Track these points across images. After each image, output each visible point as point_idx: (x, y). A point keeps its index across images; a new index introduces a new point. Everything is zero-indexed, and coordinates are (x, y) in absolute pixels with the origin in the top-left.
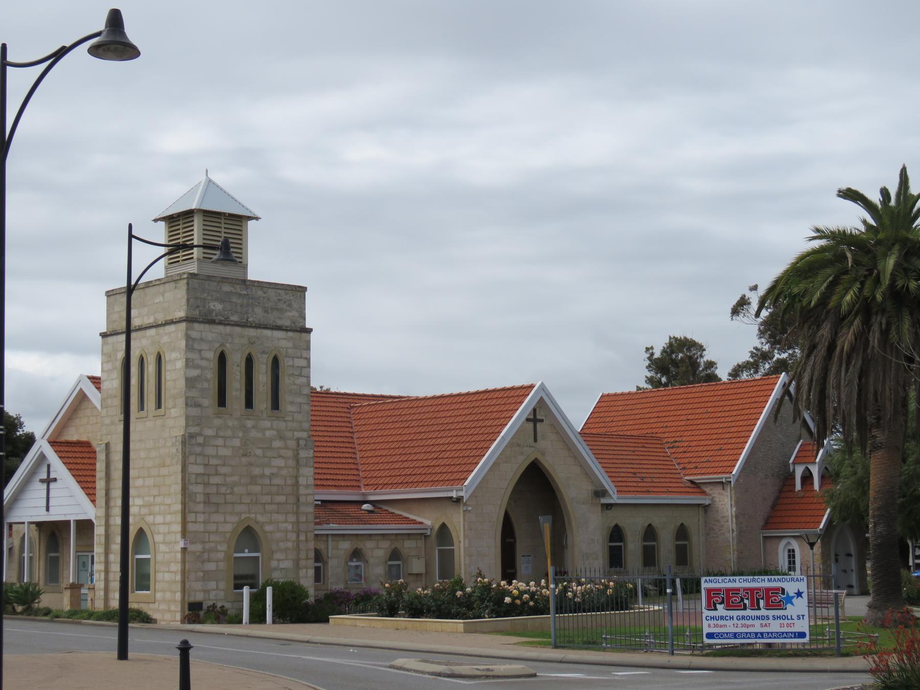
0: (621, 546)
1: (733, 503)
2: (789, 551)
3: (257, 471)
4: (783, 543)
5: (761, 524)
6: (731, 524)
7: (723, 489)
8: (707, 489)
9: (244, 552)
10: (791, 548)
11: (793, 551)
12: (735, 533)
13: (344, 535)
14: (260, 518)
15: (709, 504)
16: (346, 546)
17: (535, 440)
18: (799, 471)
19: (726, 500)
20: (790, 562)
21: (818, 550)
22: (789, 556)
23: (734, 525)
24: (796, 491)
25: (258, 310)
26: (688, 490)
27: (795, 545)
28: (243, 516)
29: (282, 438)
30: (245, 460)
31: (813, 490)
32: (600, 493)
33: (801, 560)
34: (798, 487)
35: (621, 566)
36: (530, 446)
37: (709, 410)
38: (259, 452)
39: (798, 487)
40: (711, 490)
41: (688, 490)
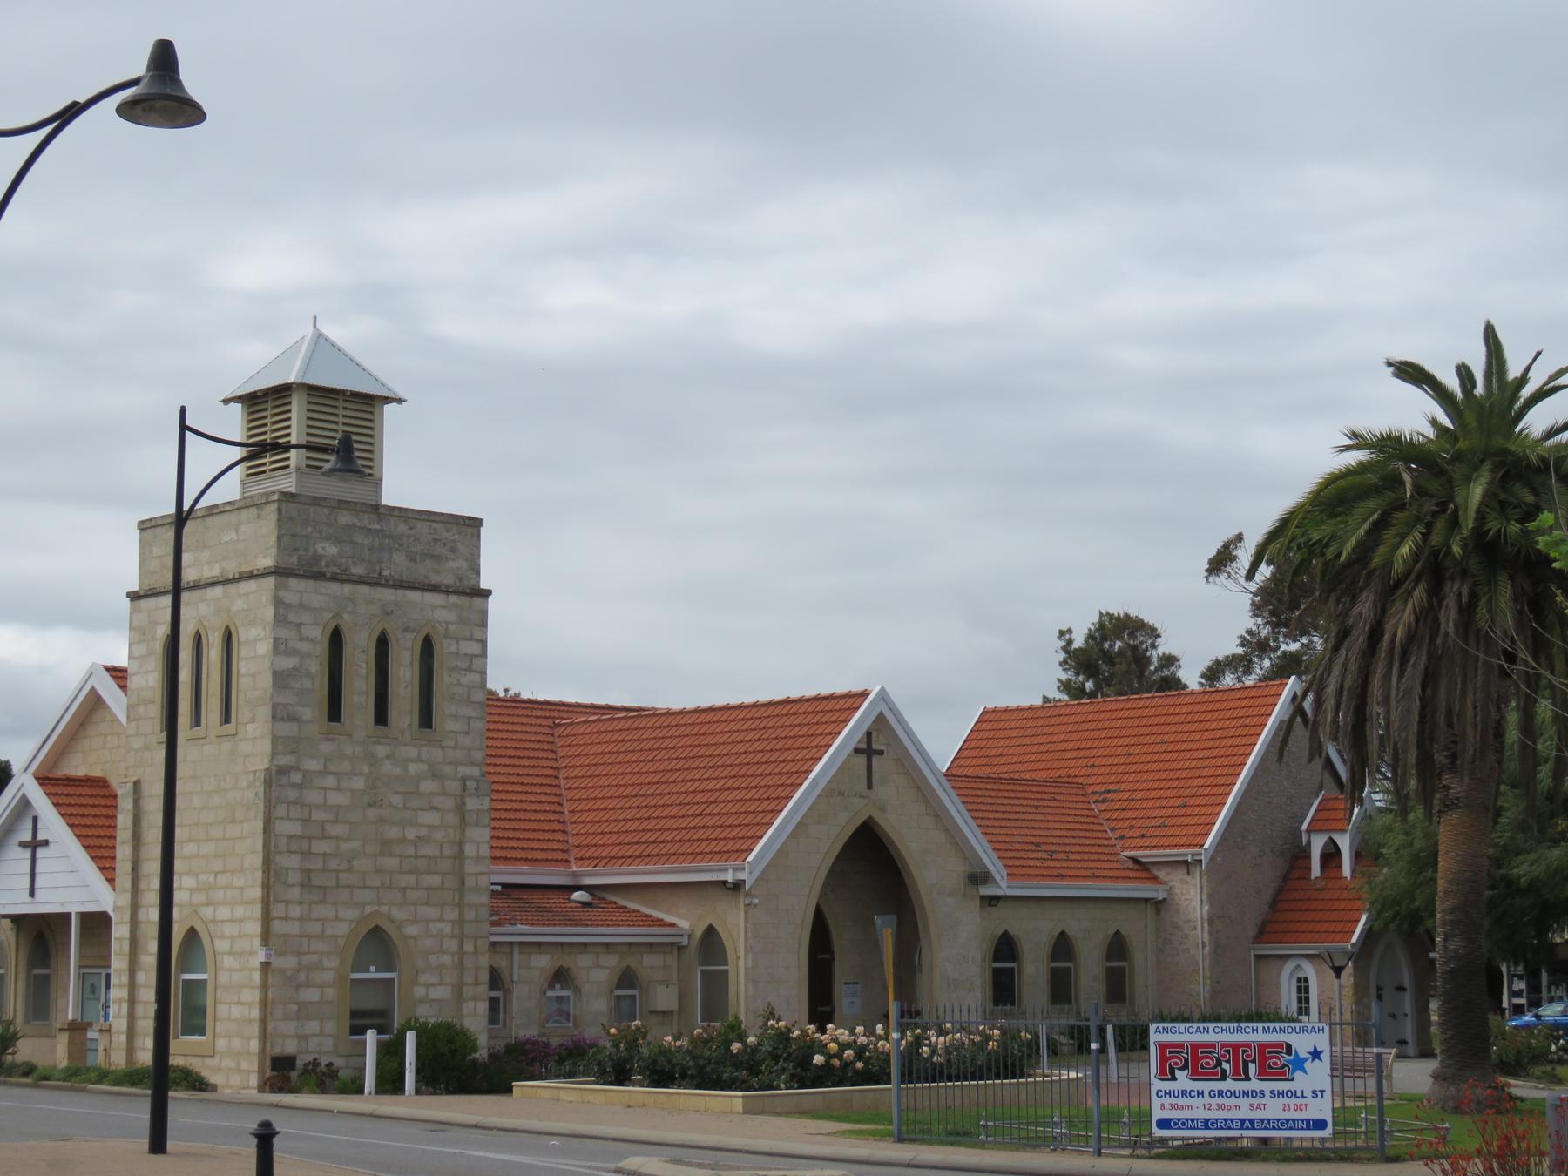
0: (1013, 969)
1: (1205, 897)
2: (1299, 980)
3: (393, 832)
4: (1290, 966)
5: (1252, 932)
6: (1201, 934)
7: (1189, 873)
8: (1161, 874)
9: (368, 971)
10: (1301, 975)
11: (1306, 980)
12: (1207, 948)
13: (539, 944)
14: (397, 914)
15: (1164, 899)
16: (543, 963)
17: (870, 786)
18: (1318, 844)
19: (1192, 892)
20: (1300, 1000)
21: (1349, 981)
22: (1299, 990)
23: (1206, 935)
24: (1312, 878)
25: (399, 558)
26: (1131, 874)
27: (1309, 970)
28: (368, 909)
29: (436, 776)
30: (372, 813)
31: (1341, 878)
32: (979, 877)
33: (1319, 995)
34: (1316, 871)
35: (1013, 1004)
36: (861, 796)
37: (1166, 738)
38: (397, 800)
39: (1316, 871)
40: (1168, 874)
41: (1131, 874)
